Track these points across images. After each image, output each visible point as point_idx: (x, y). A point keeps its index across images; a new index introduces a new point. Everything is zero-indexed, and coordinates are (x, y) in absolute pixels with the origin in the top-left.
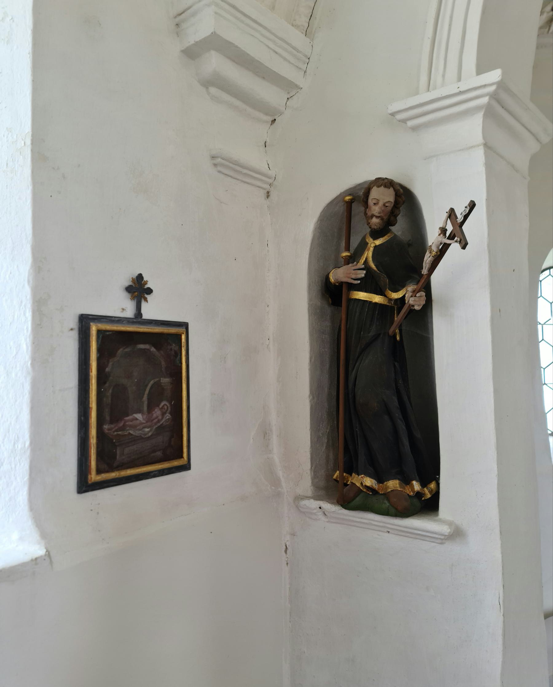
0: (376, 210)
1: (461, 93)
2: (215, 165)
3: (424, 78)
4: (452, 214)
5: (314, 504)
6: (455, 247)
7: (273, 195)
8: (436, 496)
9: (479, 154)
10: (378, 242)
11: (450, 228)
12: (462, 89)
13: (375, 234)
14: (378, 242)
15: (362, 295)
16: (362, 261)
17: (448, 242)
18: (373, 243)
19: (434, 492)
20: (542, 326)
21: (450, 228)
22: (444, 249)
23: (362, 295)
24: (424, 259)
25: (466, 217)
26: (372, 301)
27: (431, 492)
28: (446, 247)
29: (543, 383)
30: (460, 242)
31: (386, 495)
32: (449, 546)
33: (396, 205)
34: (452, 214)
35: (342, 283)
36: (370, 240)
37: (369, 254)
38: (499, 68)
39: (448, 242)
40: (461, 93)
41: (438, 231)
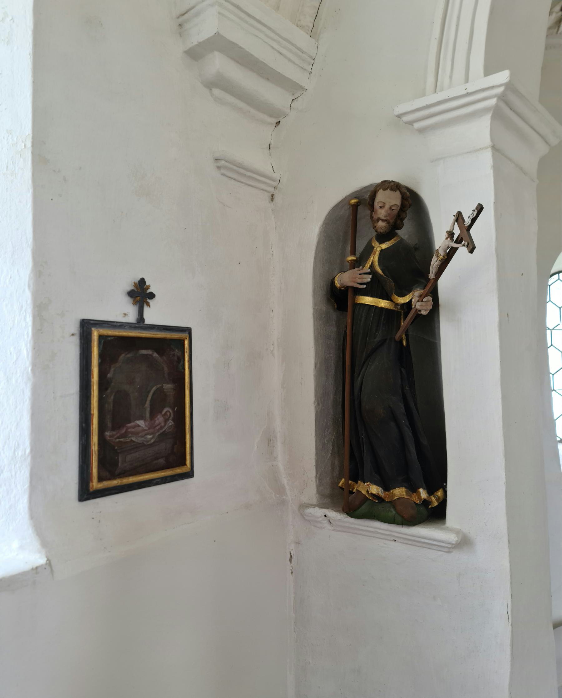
0: (382, 213)
1: (468, 94)
2: (219, 168)
3: (431, 79)
4: (459, 217)
5: (319, 512)
6: (462, 251)
7: (277, 198)
8: (443, 503)
9: (487, 157)
10: (384, 246)
11: (457, 232)
12: (469, 91)
13: (382, 238)
14: (384, 246)
15: (368, 300)
16: (368, 265)
17: (456, 245)
18: (379, 247)
19: (441, 500)
20: (551, 332)
21: (457, 232)
22: (451, 253)
23: (368, 300)
24: (431, 263)
25: (474, 220)
26: (378, 306)
27: (438, 500)
28: (453, 251)
29: (552, 389)
30: (468, 246)
31: (393, 503)
32: (456, 555)
33: (403, 208)
34: (459, 217)
35: (347, 288)
36: (376, 244)
37: (375, 258)
38: (507, 69)
39: (456, 245)
40: (468, 94)
41: (445, 235)
